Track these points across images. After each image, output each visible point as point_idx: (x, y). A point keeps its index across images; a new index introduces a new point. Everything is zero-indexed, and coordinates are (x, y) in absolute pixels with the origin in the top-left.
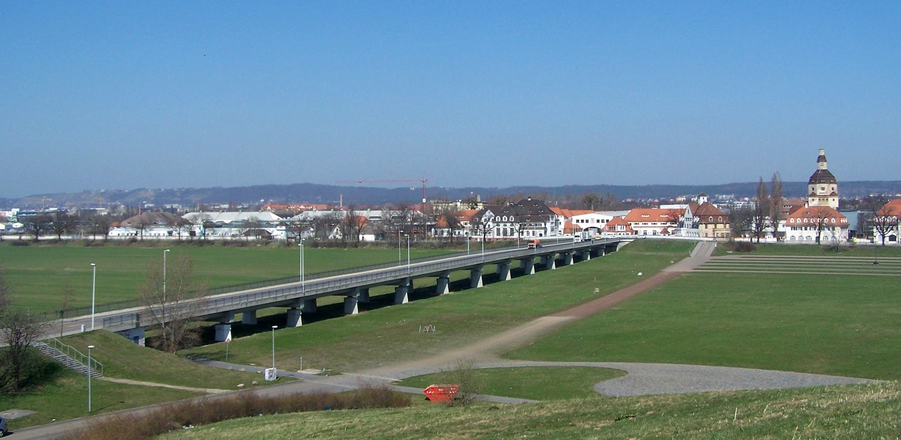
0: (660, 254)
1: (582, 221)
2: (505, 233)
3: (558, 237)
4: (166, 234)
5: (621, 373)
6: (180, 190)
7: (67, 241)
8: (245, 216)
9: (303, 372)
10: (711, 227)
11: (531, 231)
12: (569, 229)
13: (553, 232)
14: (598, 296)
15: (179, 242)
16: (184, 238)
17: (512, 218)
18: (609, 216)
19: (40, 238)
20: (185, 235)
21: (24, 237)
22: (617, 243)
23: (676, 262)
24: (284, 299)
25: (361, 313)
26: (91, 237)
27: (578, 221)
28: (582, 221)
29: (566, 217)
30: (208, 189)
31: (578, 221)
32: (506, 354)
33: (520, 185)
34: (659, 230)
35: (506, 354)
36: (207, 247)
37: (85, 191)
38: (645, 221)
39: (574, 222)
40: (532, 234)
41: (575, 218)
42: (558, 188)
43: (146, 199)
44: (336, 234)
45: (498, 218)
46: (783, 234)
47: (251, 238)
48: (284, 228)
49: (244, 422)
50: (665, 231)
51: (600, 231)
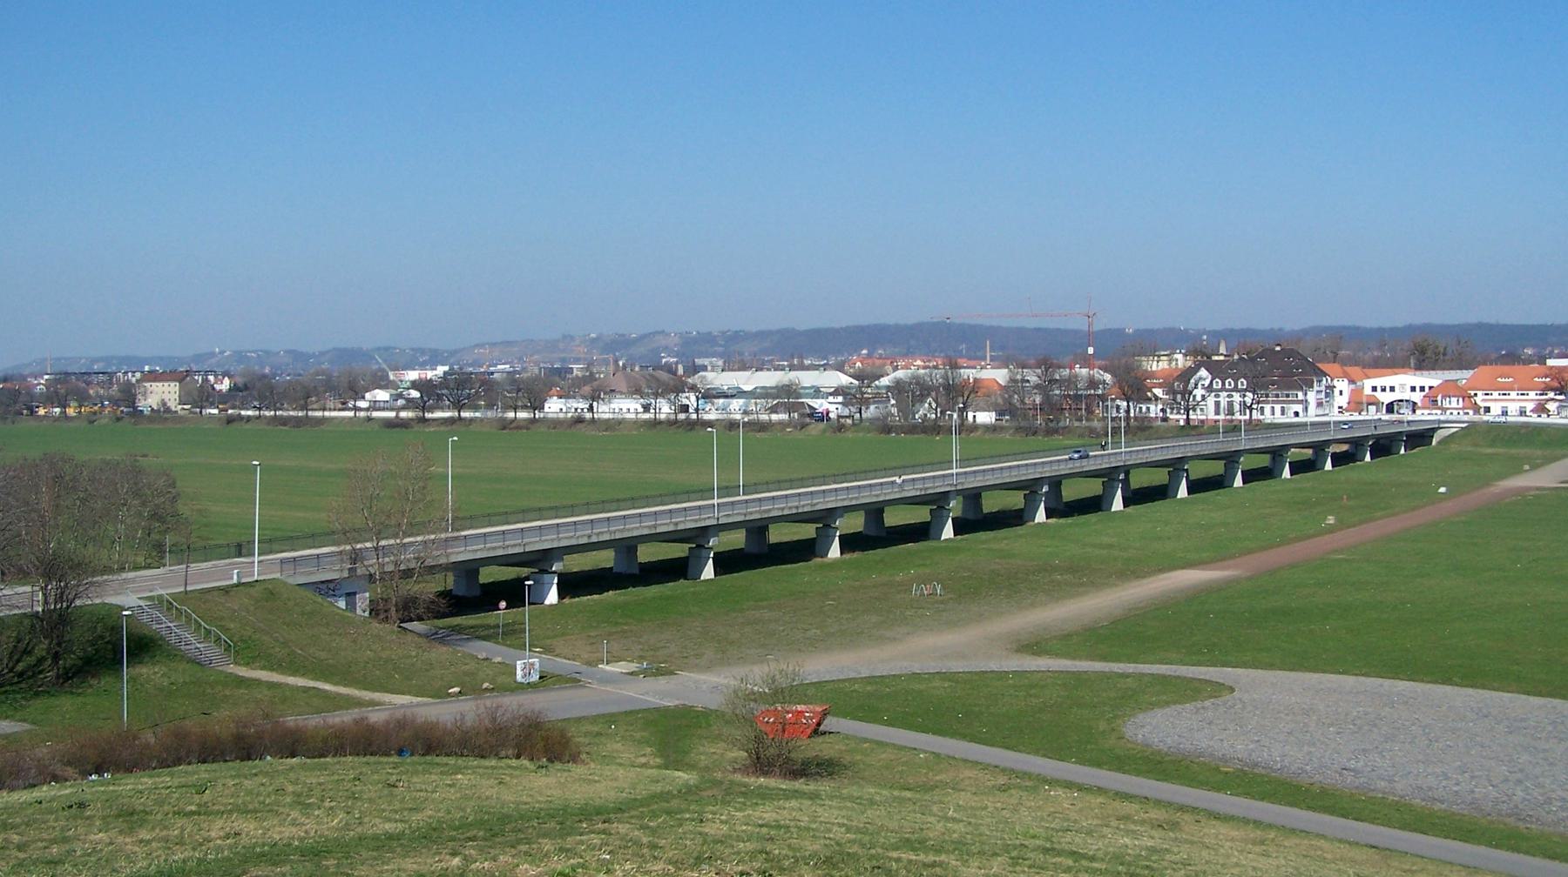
0: (1513, 451)
2: (1231, 412)
3: (1335, 416)
4: (641, 410)
5: (1219, 689)
6: (724, 333)
7: (472, 420)
8: (769, 379)
9: (608, 668)
11: (1278, 408)
12: (1357, 404)
13: (1328, 406)
14: (1331, 530)
15: (655, 423)
16: (663, 417)
17: (1243, 383)
18: (1431, 379)
19: (428, 415)
20: (665, 409)
21: (403, 414)
22: (1434, 430)
23: (1534, 467)
24: (671, 528)
25: (847, 556)
26: (511, 415)
27: (1374, 389)
28: (1384, 390)
29: (1352, 381)
30: (770, 333)
31: (1374, 389)
32: (1033, 645)
33: (1515, 322)
34: (1530, 406)
35: (1033, 645)
37: (565, 337)
39: (1368, 391)
40: (1271, 413)
41: (1368, 384)
43: (666, 348)
44: (925, 410)
45: (1218, 384)
47: (774, 417)
48: (840, 399)
50: (1541, 409)
51: (1414, 407)
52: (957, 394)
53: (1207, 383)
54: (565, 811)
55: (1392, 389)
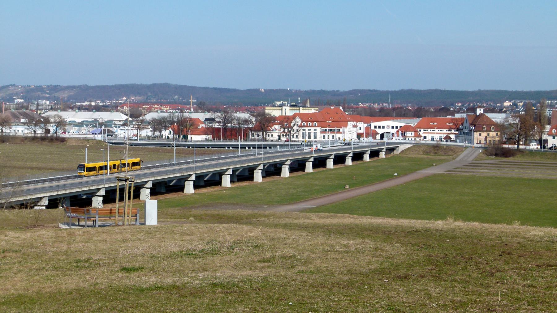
1: (379, 127)
6: (48, 86)
10: (484, 134)
16: (39, 135)
18: (400, 123)
20: (40, 132)
28: (379, 127)
30: (74, 87)
31: (375, 127)
36: (56, 144)
38: (432, 127)
39: (372, 128)
41: (373, 125)
42: (395, 92)
43: (17, 94)
46: (546, 141)
49: (332, 216)
52: (183, 127)
53: (299, 124)
54: (345, 100)
55: (383, 127)
